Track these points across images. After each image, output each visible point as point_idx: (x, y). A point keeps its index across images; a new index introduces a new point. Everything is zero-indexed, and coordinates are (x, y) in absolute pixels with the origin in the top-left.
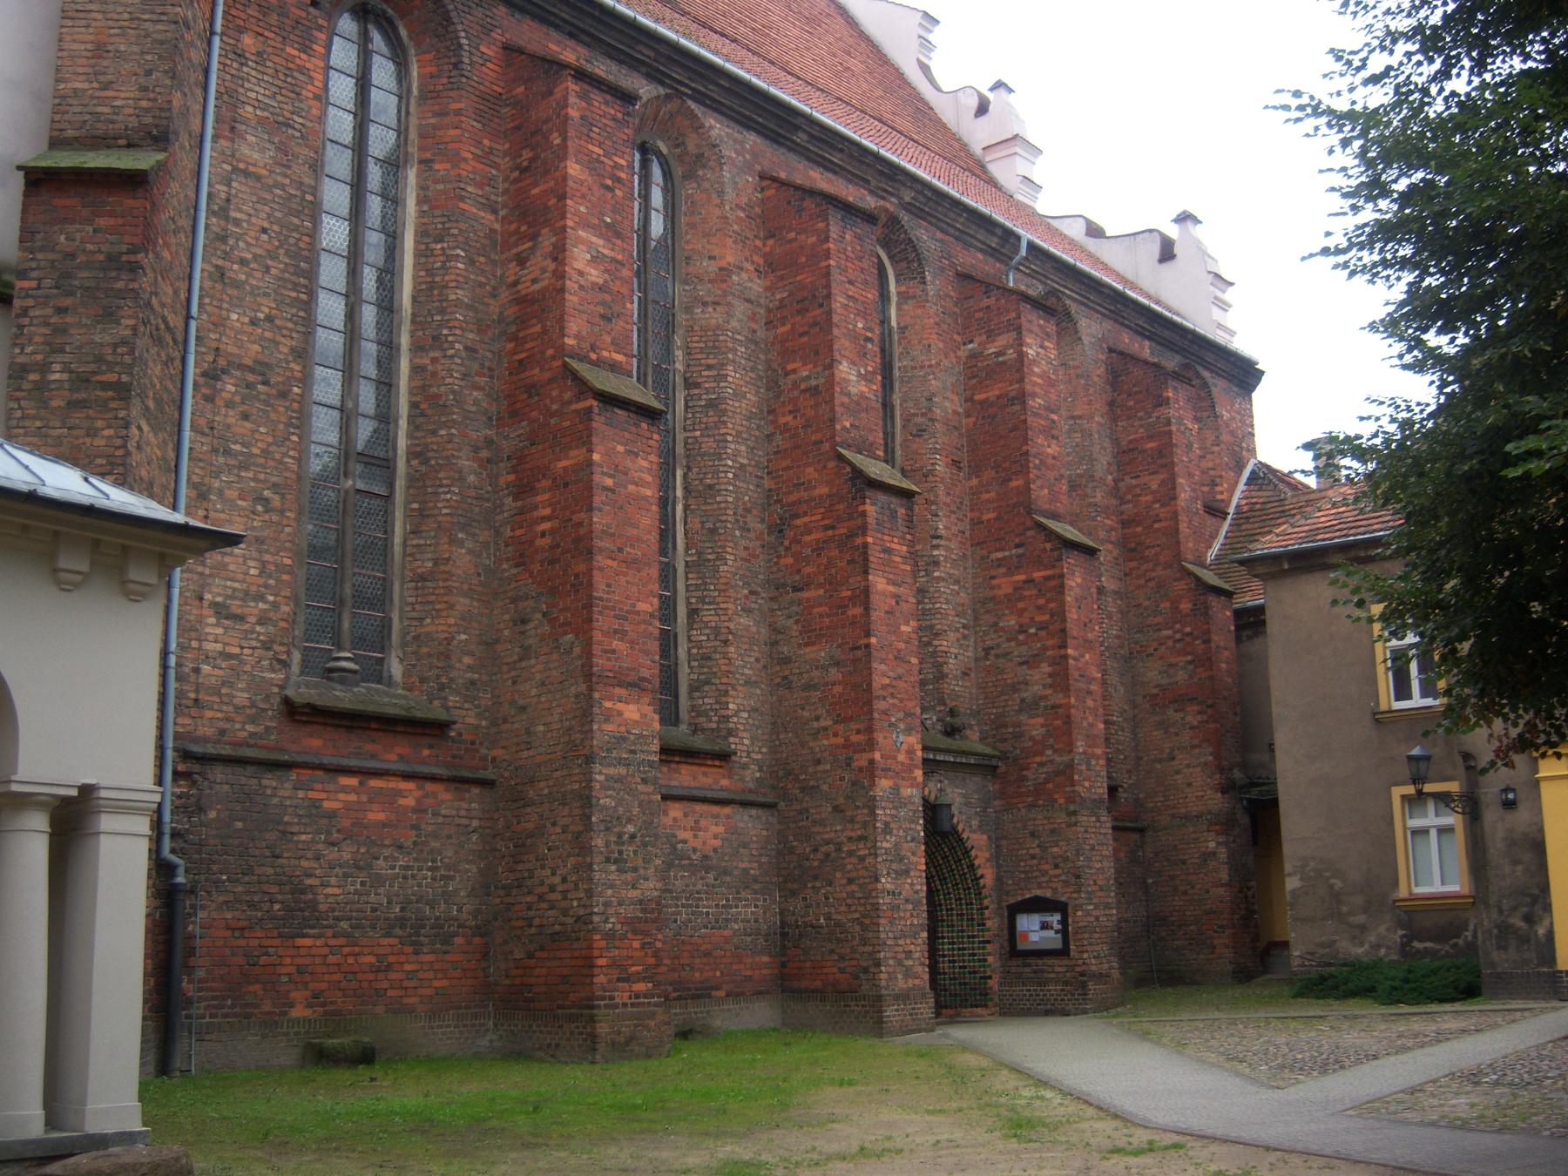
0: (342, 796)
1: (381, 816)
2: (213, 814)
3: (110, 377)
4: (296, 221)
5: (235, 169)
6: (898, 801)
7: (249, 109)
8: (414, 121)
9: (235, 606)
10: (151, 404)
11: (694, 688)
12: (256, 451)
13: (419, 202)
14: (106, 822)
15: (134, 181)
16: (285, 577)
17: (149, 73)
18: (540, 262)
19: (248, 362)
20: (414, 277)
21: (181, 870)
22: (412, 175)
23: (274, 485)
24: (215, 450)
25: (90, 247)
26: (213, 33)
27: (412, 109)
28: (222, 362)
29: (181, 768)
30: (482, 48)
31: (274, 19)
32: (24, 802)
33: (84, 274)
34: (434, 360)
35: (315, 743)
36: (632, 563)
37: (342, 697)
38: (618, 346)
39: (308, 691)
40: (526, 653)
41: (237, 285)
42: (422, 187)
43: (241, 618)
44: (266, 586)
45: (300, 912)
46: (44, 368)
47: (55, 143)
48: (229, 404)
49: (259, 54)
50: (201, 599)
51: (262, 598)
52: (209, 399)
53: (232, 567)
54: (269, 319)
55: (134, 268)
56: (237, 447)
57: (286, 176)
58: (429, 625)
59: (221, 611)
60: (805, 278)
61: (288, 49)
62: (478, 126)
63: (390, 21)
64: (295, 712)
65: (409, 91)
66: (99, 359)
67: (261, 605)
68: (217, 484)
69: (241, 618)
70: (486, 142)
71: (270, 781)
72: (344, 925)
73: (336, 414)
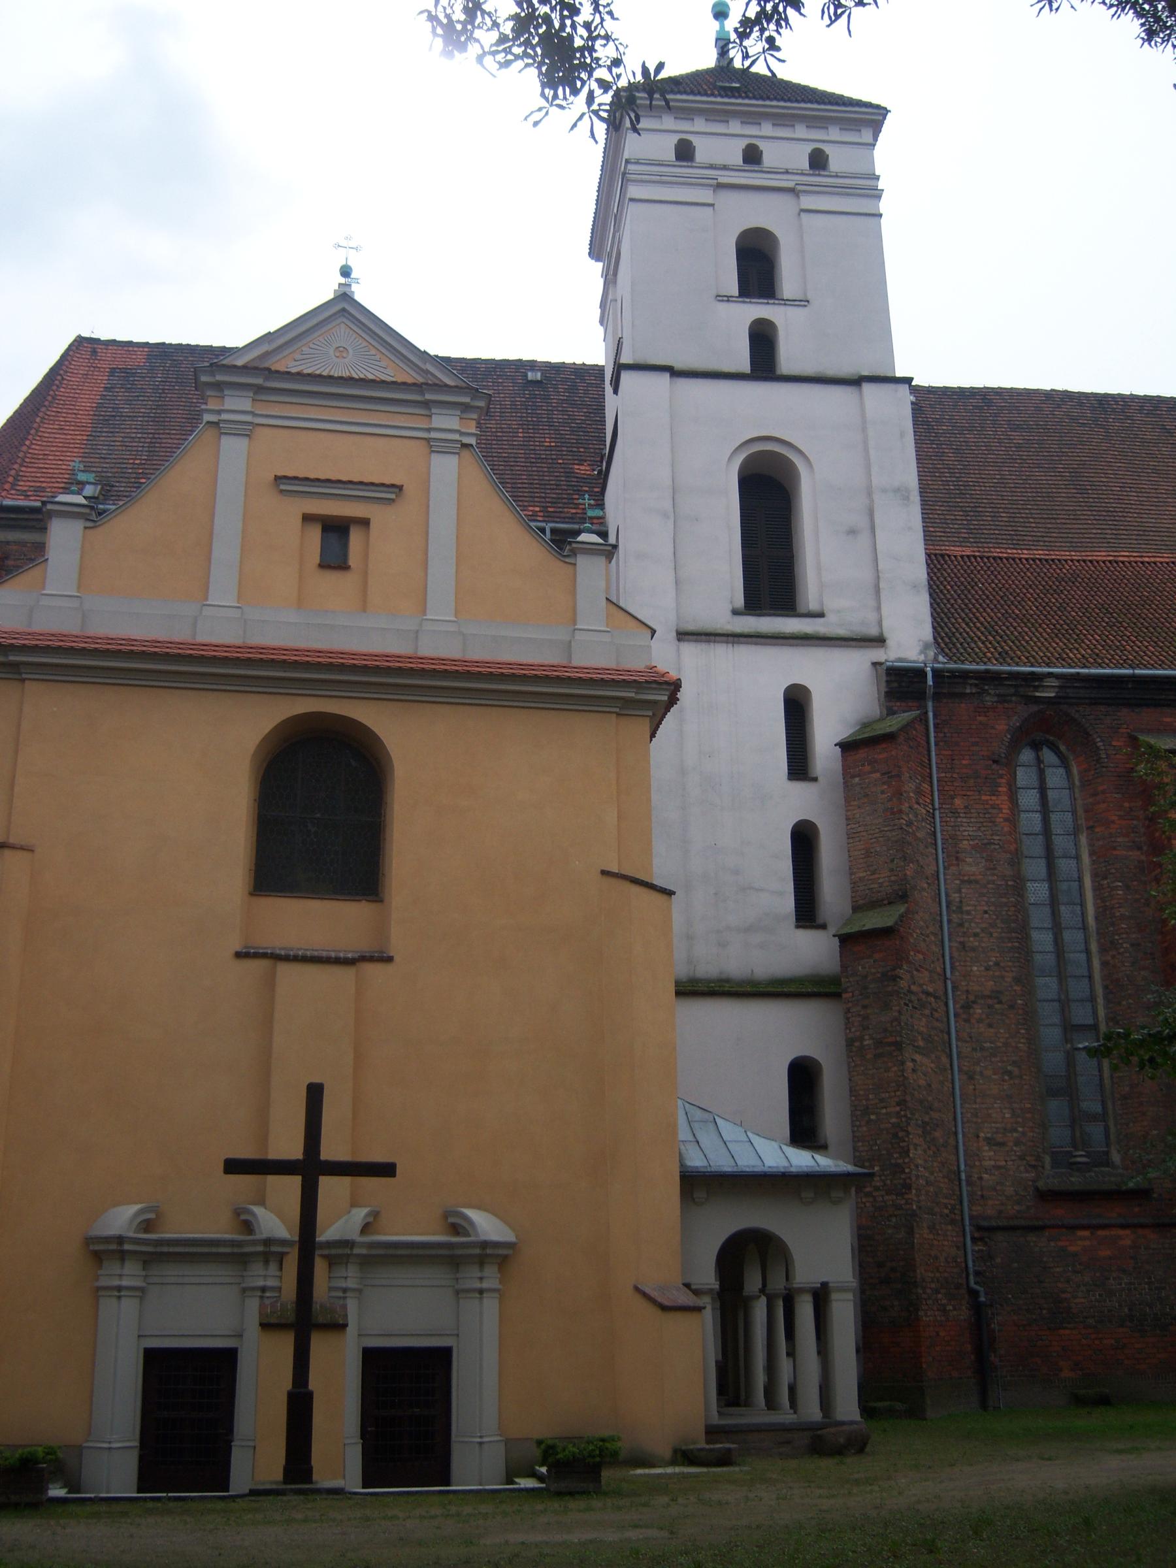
0: (1079, 1243)
1: (1108, 1253)
2: (998, 1260)
3: (890, 1039)
4: (1004, 900)
5: (963, 882)
7: (965, 842)
8: (1079, 802)
9: (999, 1138)
10: (921, 1043)
12: (1000, 1044)
13: (1091, 855)
14: (834, 1296)
16: (1028, 1115)
17: (892, 861)
19: (987, 993)
20: (1095, 904)
21: (982, 1294)
22: (1083, 839)
23: (1014, 1062)
24: (974, 1049)
25: (873, 970)
26: (934, 810)
27: (1077, 795)
28: (972, 998)
29: (976, 1235)
30: (1114, 743)
31: (971, 782)
32: (801, 1290)
33: (872, 986)
34: (1113, 957)
37: (1076, 1181)
39: (1051, 1179)
41: (973, 949)
42: (1091, 845)
43: (1003, 1144)
44: (1017, 1123)
46: (861, 1039)
47: (856, 909)
48: (980, 1021)
49: (966, 807)
50: (978, 1137)
51: (1016, 1130)
52: (967, 1021)
53: (994, 1115)
54: (997, 964)
56: (988, 1045)
57: (993, 875)
59: (990, 1141)
61: (984, 798)
62: (1119, 796)
63: (1053, 744)
64: (1047, 1196)
65: (1074, 784)
66: (885, 1030)
67: (1015, 1135)
68: (978, 1069)
69: (1003, 1144)
70: (1126, 805)
72: (1091, 1321)
73: (1056, 1004)
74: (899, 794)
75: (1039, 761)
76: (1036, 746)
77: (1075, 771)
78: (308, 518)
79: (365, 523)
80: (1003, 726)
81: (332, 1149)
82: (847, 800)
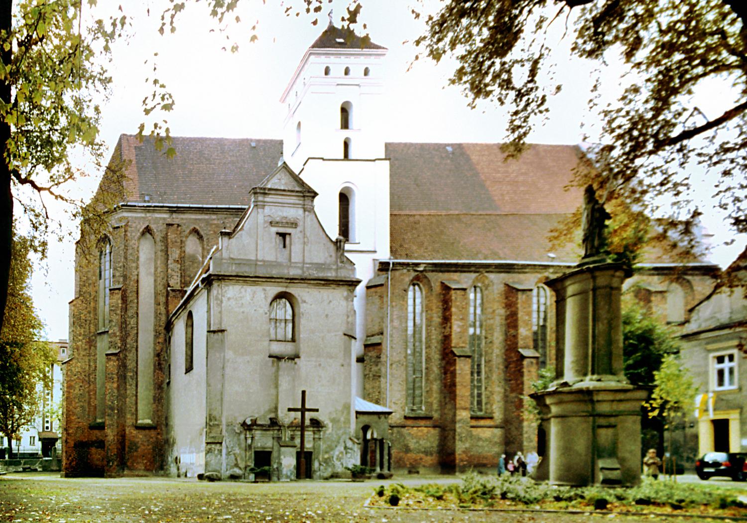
6: (529, 426)
11: (486, 404)
15: (380, 344)
18: (448, 329)
35: (409, 422)
36: (465, 387)
38: (463, 342)
40: (446, 404)
45: (407, 450)
55: (380, 358)
58: (429, 400)
59: (394, 403)
60: (513, 309)
64: (406, 418)
71: (403, 430)
74: (383, 302)
75: (414, 289)
76: (414, 285)
77: (424, 293)
78: (277, 233)
79: (290, 234)
80: (407, 279)
81: (307, 406)
82: (367, 304)
